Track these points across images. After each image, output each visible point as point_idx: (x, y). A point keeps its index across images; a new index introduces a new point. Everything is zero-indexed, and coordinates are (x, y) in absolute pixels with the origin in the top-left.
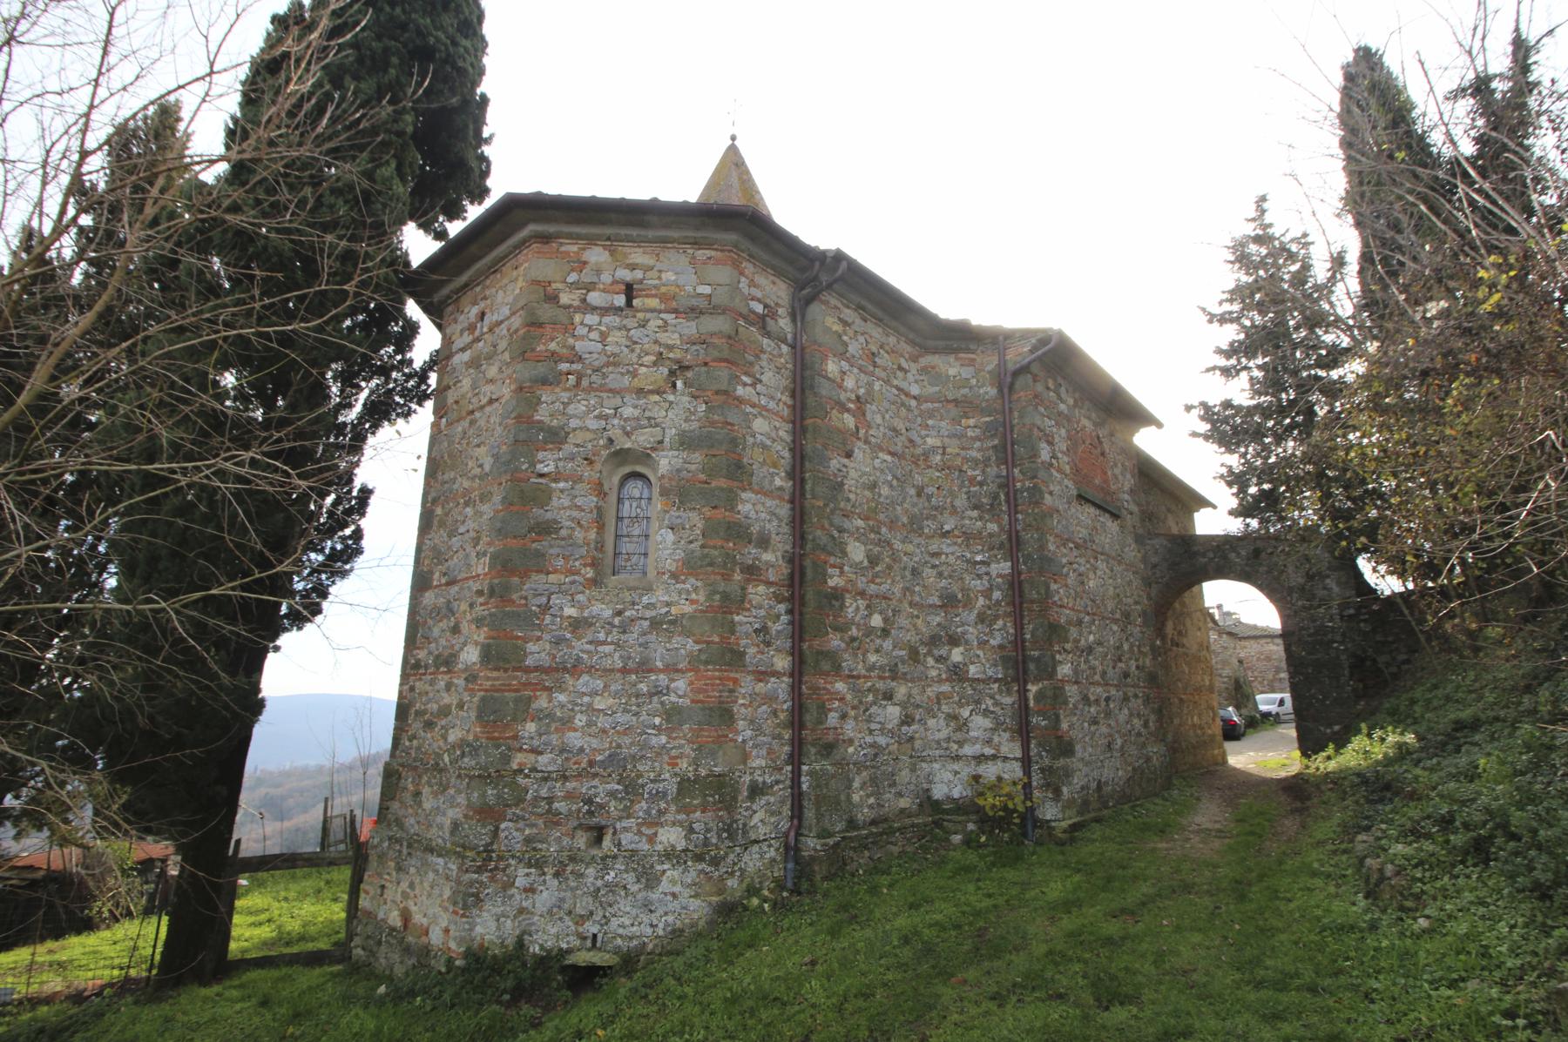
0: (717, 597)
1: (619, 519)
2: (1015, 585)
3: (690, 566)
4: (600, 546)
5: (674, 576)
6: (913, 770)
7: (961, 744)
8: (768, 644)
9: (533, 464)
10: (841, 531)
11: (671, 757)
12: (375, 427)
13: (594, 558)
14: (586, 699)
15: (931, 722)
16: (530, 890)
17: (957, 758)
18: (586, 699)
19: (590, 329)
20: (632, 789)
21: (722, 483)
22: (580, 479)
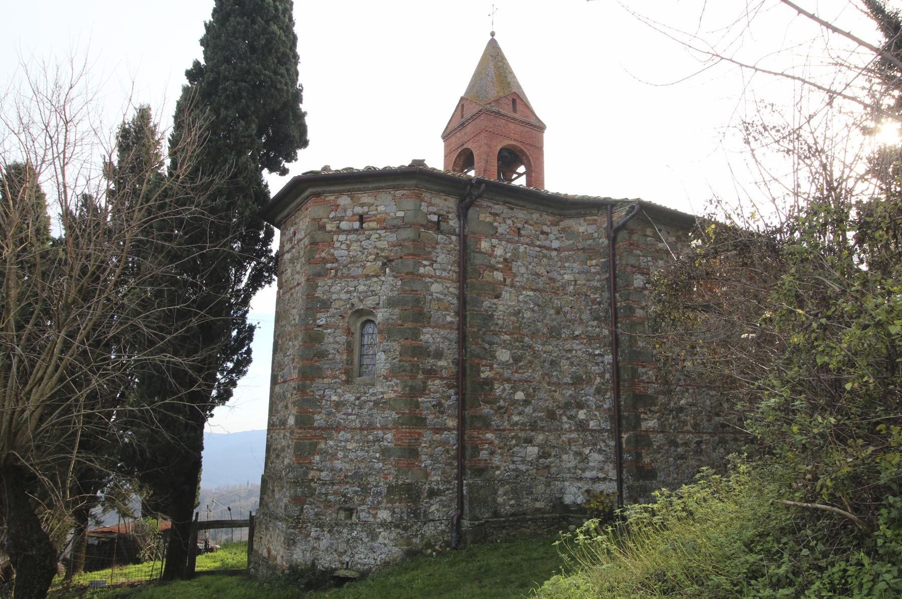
0: (407, 389)
1: (362, 345)
2: (616, 369)
3: (393, 373)
4: (350, 362)
5: (385, 378)
6: (548, 485)
7: (583, 470)
8: (443, 413)
9: (315, 320)
10: (491, 344)
11: (383, 475)
12: (255, 290)
13: (346, 369)
14: (343, 444)
15: (565, 457)
16: (317, 538)
17: (581, 479)
18: (343, 444)
19: (342, 243)
20: (365, 490)
21: (409, 325)
22: (337, 327)
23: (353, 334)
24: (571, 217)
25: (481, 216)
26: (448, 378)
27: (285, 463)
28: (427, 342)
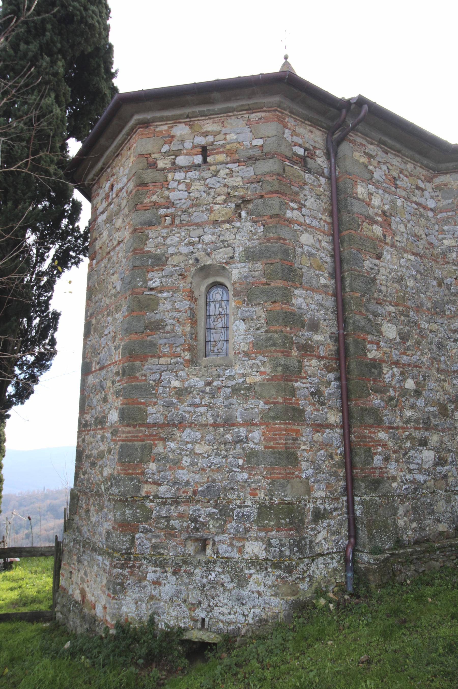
0: (280, 369)
1: (208, 316)
3: (258, 347)
5: (247, 354)
8: (322, 404)
9: (145, 282)
10: (376, 315)
11: (252, 489)
13: (190, 345)
14: (189, 446)
18: (189, 446)
19: (179, 182)
20: (224, 512)
21: (279, 283)
22: (177, 289)
23: (196, 299)
24: (447, 172)
25: (355, 153)
26: (326, 358)
27: (105, 474)
28: (299, 308)
